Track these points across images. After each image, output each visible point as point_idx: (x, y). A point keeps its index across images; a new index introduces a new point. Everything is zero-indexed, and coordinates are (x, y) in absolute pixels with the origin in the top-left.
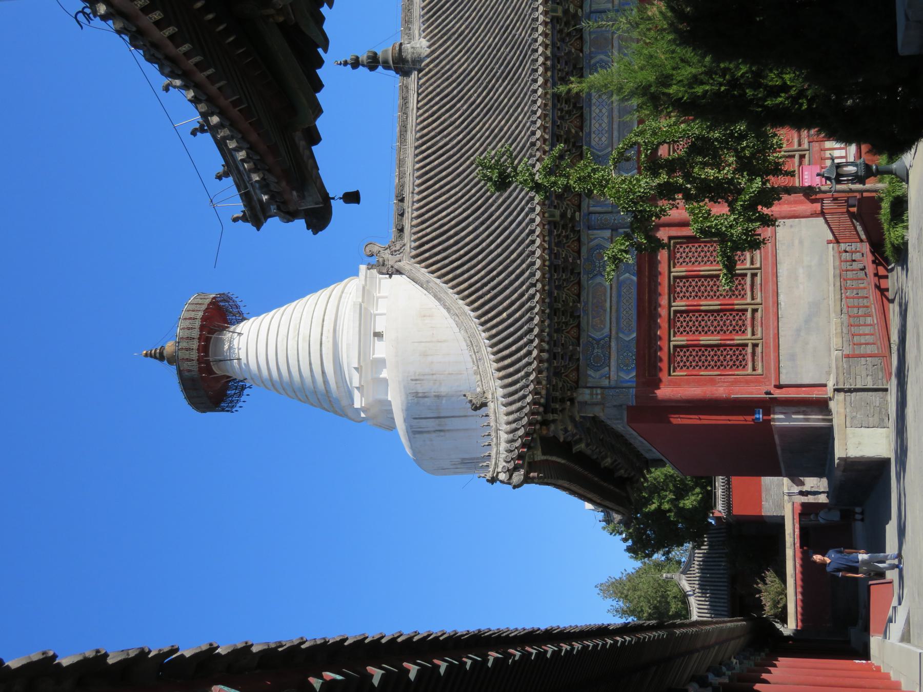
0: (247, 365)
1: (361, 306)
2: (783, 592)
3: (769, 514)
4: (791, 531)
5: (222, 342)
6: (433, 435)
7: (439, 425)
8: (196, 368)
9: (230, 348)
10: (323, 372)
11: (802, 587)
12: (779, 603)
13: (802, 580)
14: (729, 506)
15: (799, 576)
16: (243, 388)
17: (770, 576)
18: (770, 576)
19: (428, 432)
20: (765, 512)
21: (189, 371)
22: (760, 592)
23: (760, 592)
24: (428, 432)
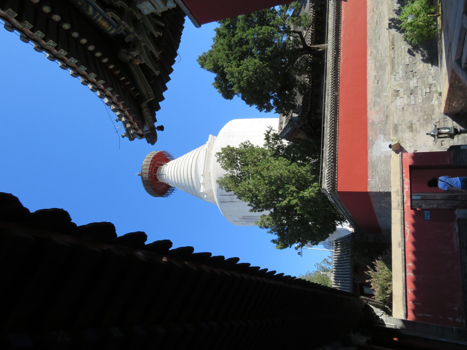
0: (168, 177)
1: (207, 150)
2: (389, 279)
3: (375, 190)
4: (399, 188)
5: (161, 168)
6: (229, 203)
7: (231, 199)
8: (147, 177)
9: (163, 171)
10: (192, 178)
11: (415, 263)
12: (387, 289)
13: (415, 253)
14: (333, 183)
15: (410, 247)
16: (174, 190)
17: (379, 264)
18: (379, 264)
19: (227, 202)
20: (368, 191)
21: (145, 178)
22: (370, 278)
23: (370, 278)
24: (227, 202)
